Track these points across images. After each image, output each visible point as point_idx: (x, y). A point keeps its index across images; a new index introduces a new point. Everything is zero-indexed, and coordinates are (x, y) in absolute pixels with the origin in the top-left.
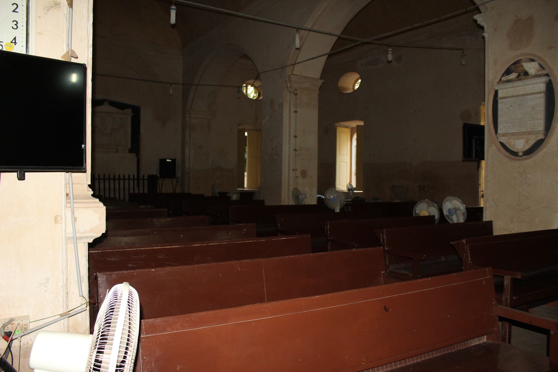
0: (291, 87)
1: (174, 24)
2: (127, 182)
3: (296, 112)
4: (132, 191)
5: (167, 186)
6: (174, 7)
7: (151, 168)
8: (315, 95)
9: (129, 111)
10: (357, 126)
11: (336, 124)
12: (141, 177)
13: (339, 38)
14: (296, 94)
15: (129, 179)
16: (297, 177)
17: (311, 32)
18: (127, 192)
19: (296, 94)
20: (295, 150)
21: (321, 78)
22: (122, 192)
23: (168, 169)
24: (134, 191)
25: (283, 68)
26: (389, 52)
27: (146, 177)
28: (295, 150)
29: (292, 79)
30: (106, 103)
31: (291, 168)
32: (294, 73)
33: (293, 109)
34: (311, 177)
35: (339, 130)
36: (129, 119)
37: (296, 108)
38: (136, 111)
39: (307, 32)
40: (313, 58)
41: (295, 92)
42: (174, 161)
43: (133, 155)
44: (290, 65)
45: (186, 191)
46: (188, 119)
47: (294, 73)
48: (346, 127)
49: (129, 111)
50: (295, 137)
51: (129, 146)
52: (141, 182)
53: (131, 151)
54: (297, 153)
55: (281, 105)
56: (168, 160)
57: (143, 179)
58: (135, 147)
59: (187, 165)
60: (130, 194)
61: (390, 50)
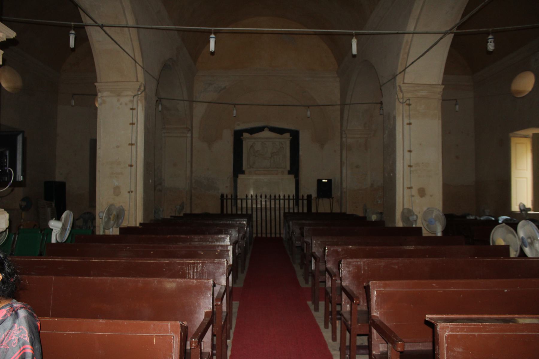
0: (403, 98)
1: (73, 48)
2: (287, 202)
3: (410, 124)
4: (287, 211)
5: (324, 206)
6: (213, 36)
7: (309, 188)
8: (436, 104)
9: (287, 135)
10: (534, 134)
11: (511, 134)
12: (300, 197)
13: (456, 35)
14: (409, 105)
15: (289, 199)
16: (413, 196)
17: (415, 35)
18: (282, 212)
19: (409, 105)
20: (410, 166)
21: (442, 84)
22: (268, 213)
23: (325, 189)
24: (294, 210)
25: (394, 77)
26: (489, 41)
27: (305, 197)
28: (410, 166)
29: (403, 89)
30: (266, 129)
31: (405, 186)
32: (406, 81)
33: (406, 121)
34: (431, 196)
35: (514, 141)
36: (288, 143)
37: (410, 119)
38: (295, 136)
39: (411, 35)
40: (413, 63)
41: (408, 102)
42: (330, 181)
43: (292, 177)
44: (400, 73)
45: (343, 211)
46: (344, 139)
47: (406, 81)
48: (525, 137)
49: (287, 135)
50: (410, 151)
51: (288, 168)
52: (300, 202)
53: (290, 173)
54: (412, 169)
55: (395, 118)
56: (324, 181)
57: (303, 199)
58: (294, 169)
59: (344, 185)
60: (285, 213)
61: (490, 37)
